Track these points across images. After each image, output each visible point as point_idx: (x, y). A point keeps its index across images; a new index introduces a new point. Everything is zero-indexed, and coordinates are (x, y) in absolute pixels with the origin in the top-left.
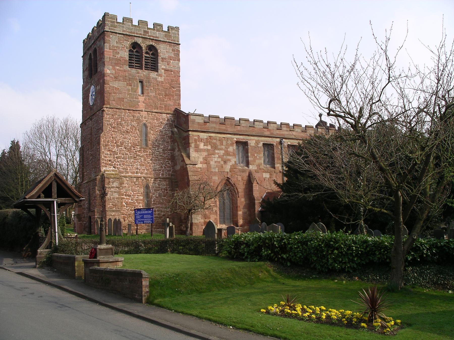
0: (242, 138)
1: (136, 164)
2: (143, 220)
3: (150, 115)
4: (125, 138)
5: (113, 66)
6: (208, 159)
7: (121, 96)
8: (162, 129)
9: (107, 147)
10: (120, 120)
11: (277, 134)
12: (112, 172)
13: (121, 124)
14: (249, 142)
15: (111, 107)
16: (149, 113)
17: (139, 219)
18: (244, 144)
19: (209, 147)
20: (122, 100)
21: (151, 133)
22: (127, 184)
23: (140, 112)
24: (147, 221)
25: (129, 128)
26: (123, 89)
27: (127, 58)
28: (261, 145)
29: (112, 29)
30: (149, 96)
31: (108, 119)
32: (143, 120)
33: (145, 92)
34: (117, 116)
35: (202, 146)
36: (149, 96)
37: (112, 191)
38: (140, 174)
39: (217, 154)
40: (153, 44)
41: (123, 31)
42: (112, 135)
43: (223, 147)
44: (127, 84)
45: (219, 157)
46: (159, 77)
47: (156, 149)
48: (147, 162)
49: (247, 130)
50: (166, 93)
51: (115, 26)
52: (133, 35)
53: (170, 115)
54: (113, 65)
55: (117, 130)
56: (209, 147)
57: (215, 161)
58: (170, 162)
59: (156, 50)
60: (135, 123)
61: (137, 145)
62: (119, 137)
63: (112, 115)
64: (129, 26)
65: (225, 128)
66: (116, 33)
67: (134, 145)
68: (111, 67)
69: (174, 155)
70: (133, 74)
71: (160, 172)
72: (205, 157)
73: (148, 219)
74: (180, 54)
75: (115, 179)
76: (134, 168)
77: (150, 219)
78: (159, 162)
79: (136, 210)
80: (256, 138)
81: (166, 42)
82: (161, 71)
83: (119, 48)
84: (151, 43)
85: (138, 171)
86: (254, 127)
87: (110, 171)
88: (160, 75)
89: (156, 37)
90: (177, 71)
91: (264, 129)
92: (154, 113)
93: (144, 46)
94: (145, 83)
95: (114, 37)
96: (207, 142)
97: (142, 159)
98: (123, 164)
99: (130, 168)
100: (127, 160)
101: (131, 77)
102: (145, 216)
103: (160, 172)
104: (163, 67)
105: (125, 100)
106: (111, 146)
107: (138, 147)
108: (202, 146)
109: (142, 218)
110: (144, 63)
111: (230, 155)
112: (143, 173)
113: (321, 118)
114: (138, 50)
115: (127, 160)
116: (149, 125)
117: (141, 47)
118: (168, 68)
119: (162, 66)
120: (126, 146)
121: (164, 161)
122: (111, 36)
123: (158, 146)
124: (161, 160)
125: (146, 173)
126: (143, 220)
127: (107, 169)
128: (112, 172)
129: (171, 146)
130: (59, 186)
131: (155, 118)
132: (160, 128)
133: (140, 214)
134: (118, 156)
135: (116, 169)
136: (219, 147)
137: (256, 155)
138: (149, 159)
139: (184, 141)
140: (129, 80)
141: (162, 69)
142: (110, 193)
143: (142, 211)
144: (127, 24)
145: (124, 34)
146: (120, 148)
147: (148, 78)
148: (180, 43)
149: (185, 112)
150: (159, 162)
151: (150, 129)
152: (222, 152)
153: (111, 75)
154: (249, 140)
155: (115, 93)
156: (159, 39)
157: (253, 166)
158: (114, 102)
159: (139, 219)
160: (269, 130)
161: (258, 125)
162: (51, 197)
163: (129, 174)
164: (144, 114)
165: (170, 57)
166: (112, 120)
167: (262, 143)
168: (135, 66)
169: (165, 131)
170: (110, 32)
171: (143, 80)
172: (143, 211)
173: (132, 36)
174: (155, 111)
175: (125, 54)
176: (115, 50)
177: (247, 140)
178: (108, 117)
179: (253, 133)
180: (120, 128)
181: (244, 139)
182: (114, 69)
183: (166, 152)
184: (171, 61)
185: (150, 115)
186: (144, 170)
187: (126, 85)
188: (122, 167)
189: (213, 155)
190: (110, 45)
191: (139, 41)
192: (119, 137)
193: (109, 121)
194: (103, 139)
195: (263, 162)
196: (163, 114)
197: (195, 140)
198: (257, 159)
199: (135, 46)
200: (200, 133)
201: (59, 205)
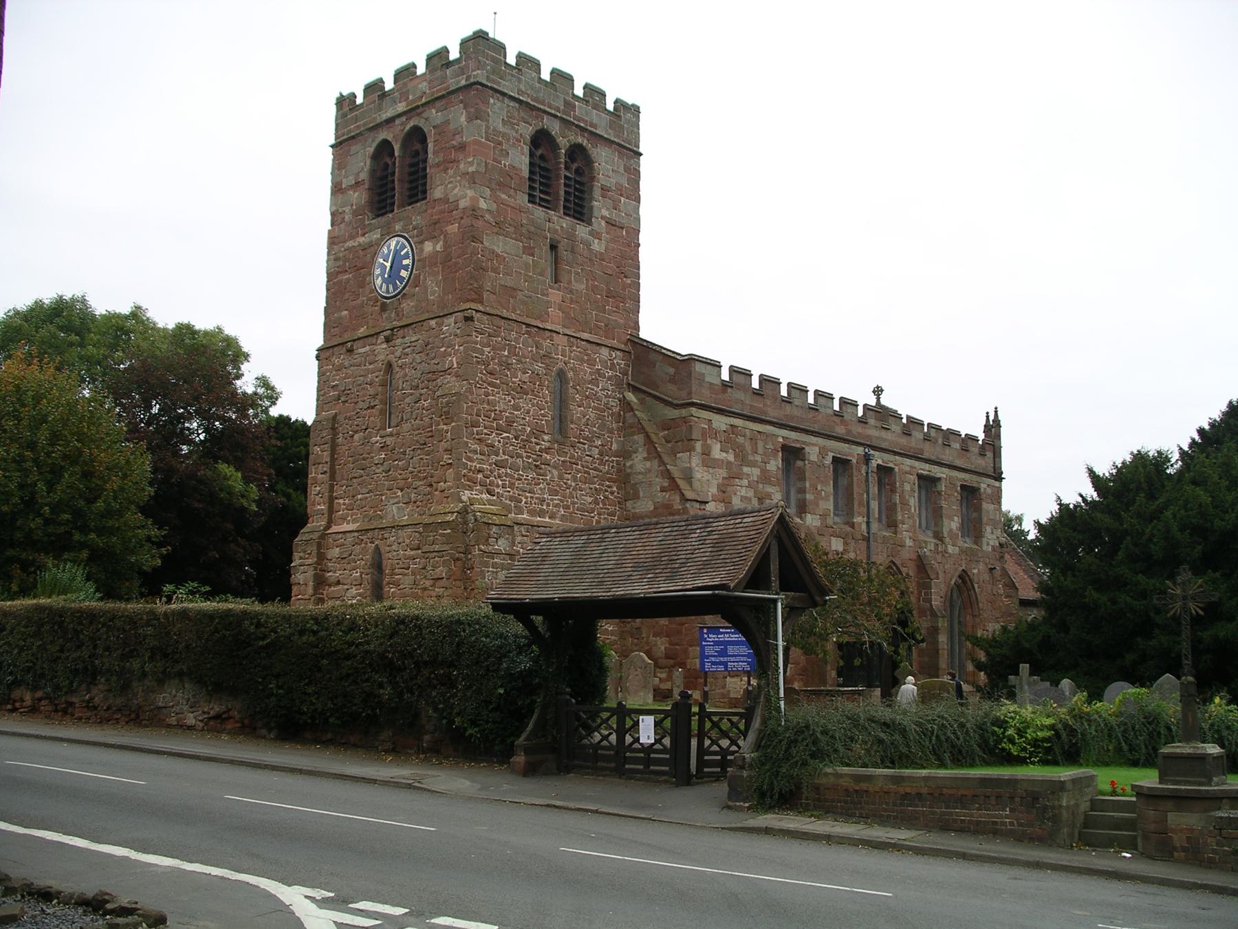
0: (794, 438)
1: (541, 489)
2: (726, 659)
3: (575, 348)
4: (516, 408)
5: (492, 190)
6: (729, 489)
7: (509, 282)
8: (601, 390)
9: (475, 429)
10: (506, 353)
11: (858, 433)
12: (488, 506)
13: (508, 366)
14: (807, 449)
15: (488, 310)
16: (572, 339)
17: (715, 656)
18: (792, 454)
19: (731, 458)
20: (511, 291)
21: (574, 397)
22: (520, 545)
23: (554, 335)
24: (736, 664)
25: (526, 377)
26: (515, 261)
27: (526, 174)
28: (828, 460)
29: (493, 81)
30: (571, 292)
31: (478, 346)
32: (558, 359)
33: (564, 278)
34: (500, 339)
35: (716, 452)
36: (571, 292)
37: (496, 563)
38: (550, 518)
39: (745, 476)
40: (585, 143)
41: (520, 92)
42: (487, 394)
43: (759, 458)
44: (524, 247)
45: (749, 486)
46: (596, 241)
47: (586, 446)
48: (566, 484)
49: (804, 416)
50: (609, 291)
51: (501, 73)
52: (542, 107)
53: (618, 353)
54: (494, 186)
55: (498, 382)
56: (731, 458)
57: (741, 496)
58: (615, 489)
59: (589, 161)
60: (540, 365)
61: (543, 432)
62: (502, 401)
63: (489, 336)
64: (533, 79)
65: (761, 405)
66: (504, 94)
67: (537, 432)
68: (488, 192)
69: (628, 471)
70: (539, 220)
71: (593, 517)
72: (723, 485)
73: (738, 659)
74: (641, 182)
75: (502, 527)
76: (536, 498)
77: (745, 659)
78: (591, 486)
79: (705, 631)
80: (820, 441)
81: (613, 142)
82: (599, 225)
83: (509, 140)
84: (580, 140)
85: (544, 507)
86: (817, 410)
87: (485, 505)
88: (596, 235)
89: (592, 125)
90: (634, 229)
91: (835, 417)
92: (584, 343)
93: (563, 143)
94: (564, 254)
95: (499, 104)
96: (729, 439)
97: (555, 473)
98: (512, 485)
99: (526, 498)
100: (521, 472)
101: (532, 229)
102: (731, 650)
103: (593, 517)
104: (605, 213)
105: (520, 295)
106: (485, 428)
107: (546, 438)
108: (716, 452)
109: (723, 653)
110: (562, 193)
111: (770, 483)
112: (555, 513)
113: (878, 399)
114: (545, 153)
115: (521, 472)
116: (570, 374)
117: (554, 146)
118: (614, 215)
119: (600, 208)
120: (520, 431)
121: (603, 485)
122: (492, 101)
123: (591, 440)
124: (596, 479)
125: (563, 515)
126: (726, 659)
127: (476, 496)
128: (488, 506)
129: (618, 442)
130: (783, 552)
131: (586, 358)
132: (595, 388)
133: (716, 643)
134: (499, 458)
135: (494, 498)
136: (751, 458)
137: (819, 488)
138: (570, 476)
139: (667, 432)
140: (528, 237)
141: (603, 217)
142: (491, 569)
143: (722, 633)
144: (528, 73)
145: (520, 102)
146: (505, 435)
147: (572, 237)
148: (641, 150)
149: (672, 349)
150: (591, 486)
151: (574, 387)
152: (755, 472)
153: (487, 216)
154: (808, 445)
155: (496, 271)
156: (597, 132)
157: (814, 516)
158: (494, 297)
159: (715, 656)
160: (844, 422)
161: (825, 407)
162: (767, 588)
163: (525, 516)
164: (560, 340)
165: (619, 188)
166: (488, 349)
167: (831, 455)
168: (541, 199)
169: (606, 397)
170: (492, 88)
171: (559, 242)
172: (724, 633)
173: (539, 109)
174: (585, 336)
175: (520, 159)
176: (500, 144)
177: (804, 443)
178: (479, 339)
179: (816, 426)
180: (507, 376)
181: (797, 440)
182: (496, 199)
183: (607, 458)
184: (622, 199)
185: (575, 348)
186: (557, 506)
187: (521, 252)
188: (509, 492)
189: (737, 480)
190: (488, 128)
191: (555, 128)
192: (502, 401)
193: (482, 353)
194: (465, 405)
195: (832, 508)
196: (603, 348)
197: (704, 433)
198: (822, 499)
199: (541, 139)
200: (715, 415)
201: (790, 611)
